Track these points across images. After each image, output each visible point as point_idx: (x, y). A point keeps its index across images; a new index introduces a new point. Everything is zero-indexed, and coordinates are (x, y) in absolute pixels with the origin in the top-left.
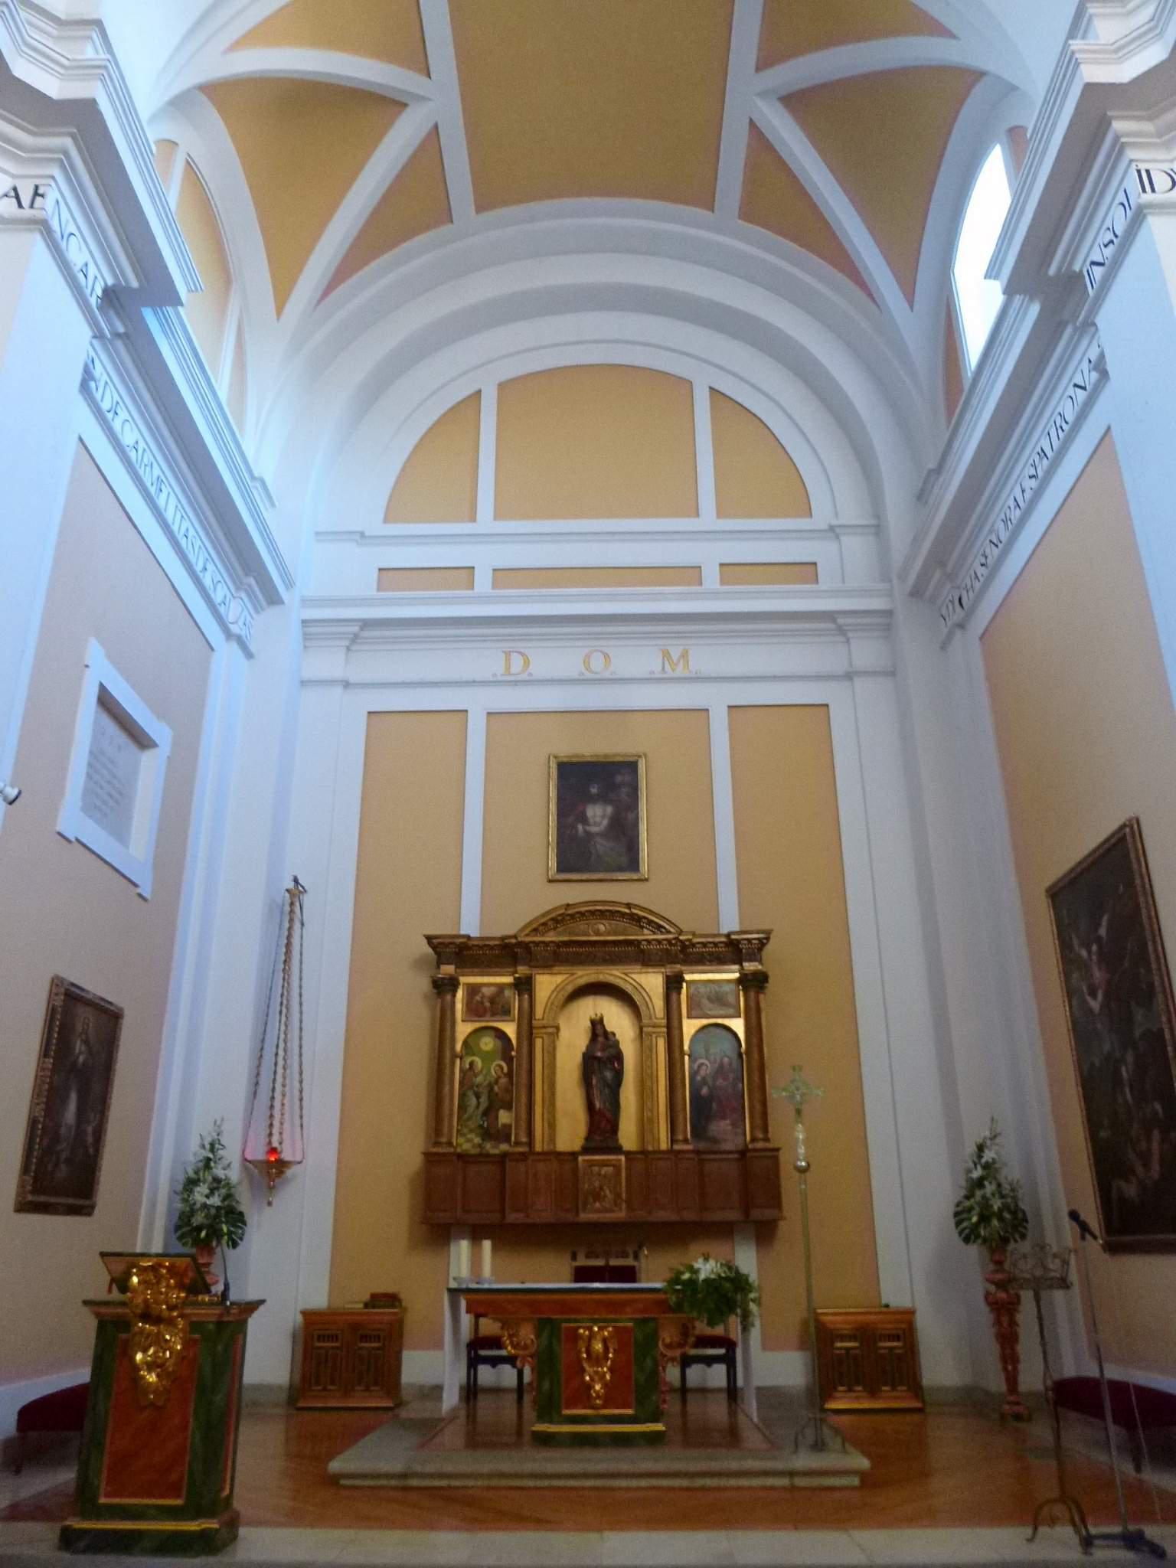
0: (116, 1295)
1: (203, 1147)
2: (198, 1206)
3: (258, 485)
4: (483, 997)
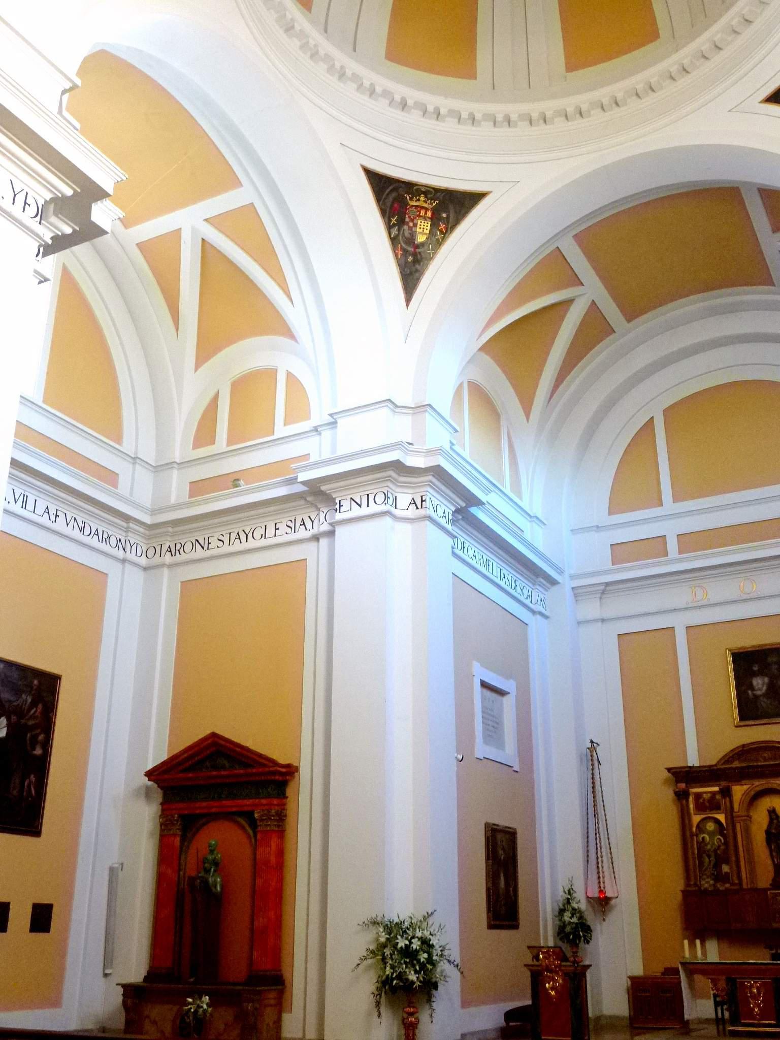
0: (536, 963)
1: (565, 892)
2: (567, 922)
3: (535, 519)
4: (704, 800)
